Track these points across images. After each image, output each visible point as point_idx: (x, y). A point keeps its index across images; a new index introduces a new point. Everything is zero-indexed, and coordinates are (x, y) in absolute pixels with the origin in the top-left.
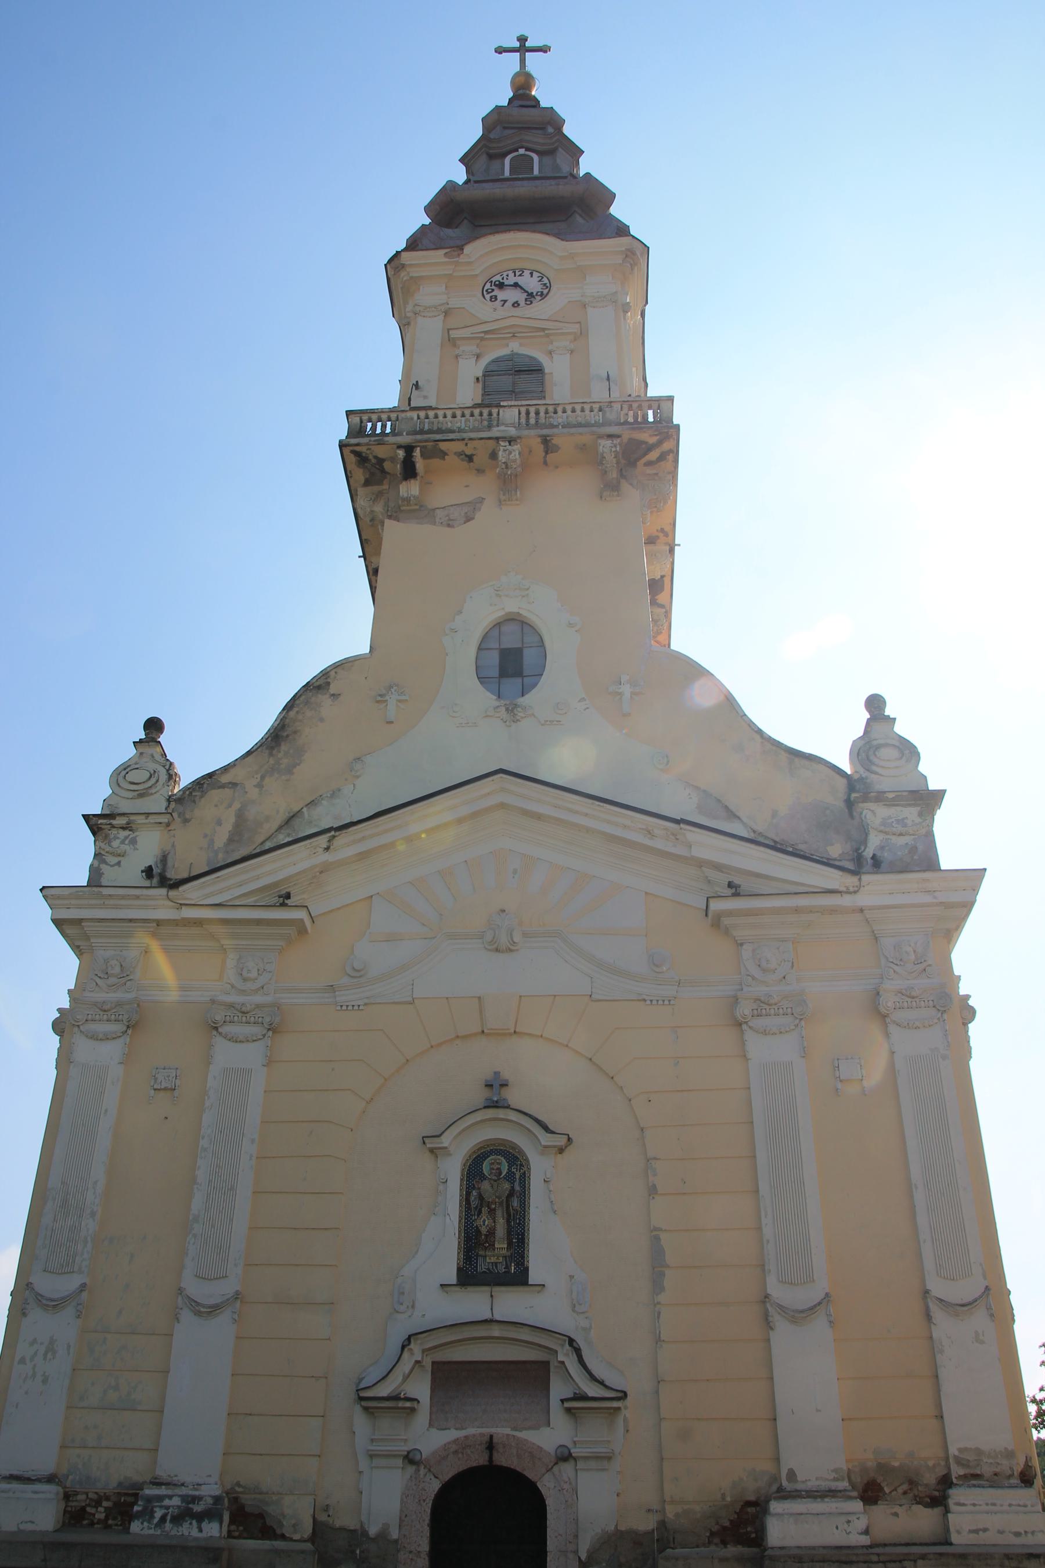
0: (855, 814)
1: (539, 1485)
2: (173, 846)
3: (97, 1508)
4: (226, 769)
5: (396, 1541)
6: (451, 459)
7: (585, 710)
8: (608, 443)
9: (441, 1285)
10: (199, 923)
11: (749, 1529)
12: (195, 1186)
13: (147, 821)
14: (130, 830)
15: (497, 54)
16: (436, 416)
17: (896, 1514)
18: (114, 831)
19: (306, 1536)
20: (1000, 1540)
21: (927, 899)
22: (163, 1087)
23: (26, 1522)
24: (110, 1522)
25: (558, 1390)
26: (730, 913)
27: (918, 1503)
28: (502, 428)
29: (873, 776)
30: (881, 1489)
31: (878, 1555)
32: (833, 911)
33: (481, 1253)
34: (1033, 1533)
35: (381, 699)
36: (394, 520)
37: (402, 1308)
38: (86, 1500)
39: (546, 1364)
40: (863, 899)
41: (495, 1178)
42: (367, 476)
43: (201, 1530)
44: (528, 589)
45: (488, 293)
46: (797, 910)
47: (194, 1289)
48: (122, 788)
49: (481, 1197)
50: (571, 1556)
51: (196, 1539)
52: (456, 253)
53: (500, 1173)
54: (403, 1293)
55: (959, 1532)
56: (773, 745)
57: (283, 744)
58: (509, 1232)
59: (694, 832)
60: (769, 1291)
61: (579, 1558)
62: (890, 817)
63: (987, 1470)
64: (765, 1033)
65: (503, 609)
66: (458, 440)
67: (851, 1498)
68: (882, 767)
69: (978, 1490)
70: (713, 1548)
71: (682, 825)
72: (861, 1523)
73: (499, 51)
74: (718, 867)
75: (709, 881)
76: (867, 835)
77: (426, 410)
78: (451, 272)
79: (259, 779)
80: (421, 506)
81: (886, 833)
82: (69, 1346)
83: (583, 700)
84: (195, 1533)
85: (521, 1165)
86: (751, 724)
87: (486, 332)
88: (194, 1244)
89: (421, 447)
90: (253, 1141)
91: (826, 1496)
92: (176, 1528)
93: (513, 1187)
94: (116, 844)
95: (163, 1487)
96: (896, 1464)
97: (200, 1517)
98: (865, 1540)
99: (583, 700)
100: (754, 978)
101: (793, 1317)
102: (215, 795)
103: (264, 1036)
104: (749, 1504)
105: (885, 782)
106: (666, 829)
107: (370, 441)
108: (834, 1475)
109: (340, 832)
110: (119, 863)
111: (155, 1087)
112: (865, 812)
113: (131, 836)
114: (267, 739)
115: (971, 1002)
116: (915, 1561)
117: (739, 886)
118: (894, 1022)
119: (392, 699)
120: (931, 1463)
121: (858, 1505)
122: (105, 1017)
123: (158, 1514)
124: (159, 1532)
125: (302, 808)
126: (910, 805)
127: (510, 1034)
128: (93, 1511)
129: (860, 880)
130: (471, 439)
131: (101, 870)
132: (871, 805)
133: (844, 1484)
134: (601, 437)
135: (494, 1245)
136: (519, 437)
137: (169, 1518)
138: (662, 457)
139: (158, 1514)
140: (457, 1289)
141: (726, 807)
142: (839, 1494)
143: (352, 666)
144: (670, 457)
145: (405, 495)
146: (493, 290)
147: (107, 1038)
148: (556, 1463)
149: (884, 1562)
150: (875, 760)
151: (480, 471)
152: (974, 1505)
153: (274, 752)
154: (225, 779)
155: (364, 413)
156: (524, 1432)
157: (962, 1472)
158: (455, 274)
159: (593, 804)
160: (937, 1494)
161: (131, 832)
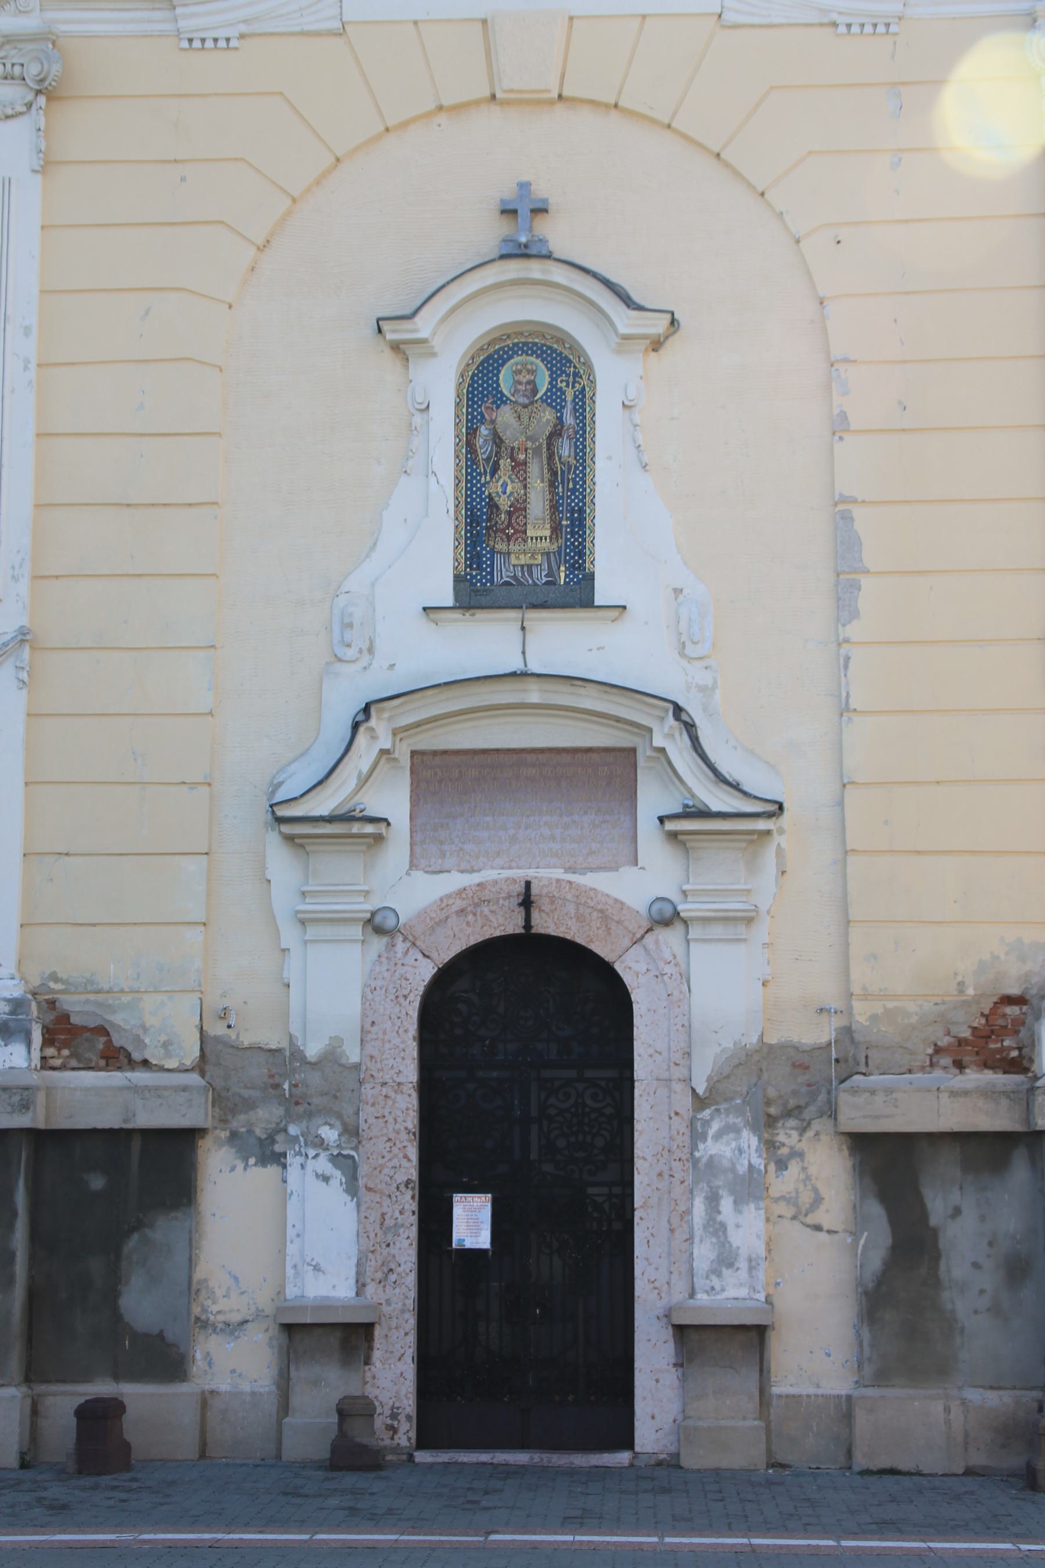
5: (357, 1067)
9: (425, 609)
11: (1006, 1043)
33: (501, 546)
37: (350, 653)
49: (497, 440)
50: (678, 1087)
53: (535, 391)
54: (350, 625)
61: (693, 1090)
70: (938, 1073)
85: (576, 375)
90: (27, 331)
93: (560, 419)
103: (29, 106)
104: (1008, 1000)
127: (550, 103)
140: (457, 615)
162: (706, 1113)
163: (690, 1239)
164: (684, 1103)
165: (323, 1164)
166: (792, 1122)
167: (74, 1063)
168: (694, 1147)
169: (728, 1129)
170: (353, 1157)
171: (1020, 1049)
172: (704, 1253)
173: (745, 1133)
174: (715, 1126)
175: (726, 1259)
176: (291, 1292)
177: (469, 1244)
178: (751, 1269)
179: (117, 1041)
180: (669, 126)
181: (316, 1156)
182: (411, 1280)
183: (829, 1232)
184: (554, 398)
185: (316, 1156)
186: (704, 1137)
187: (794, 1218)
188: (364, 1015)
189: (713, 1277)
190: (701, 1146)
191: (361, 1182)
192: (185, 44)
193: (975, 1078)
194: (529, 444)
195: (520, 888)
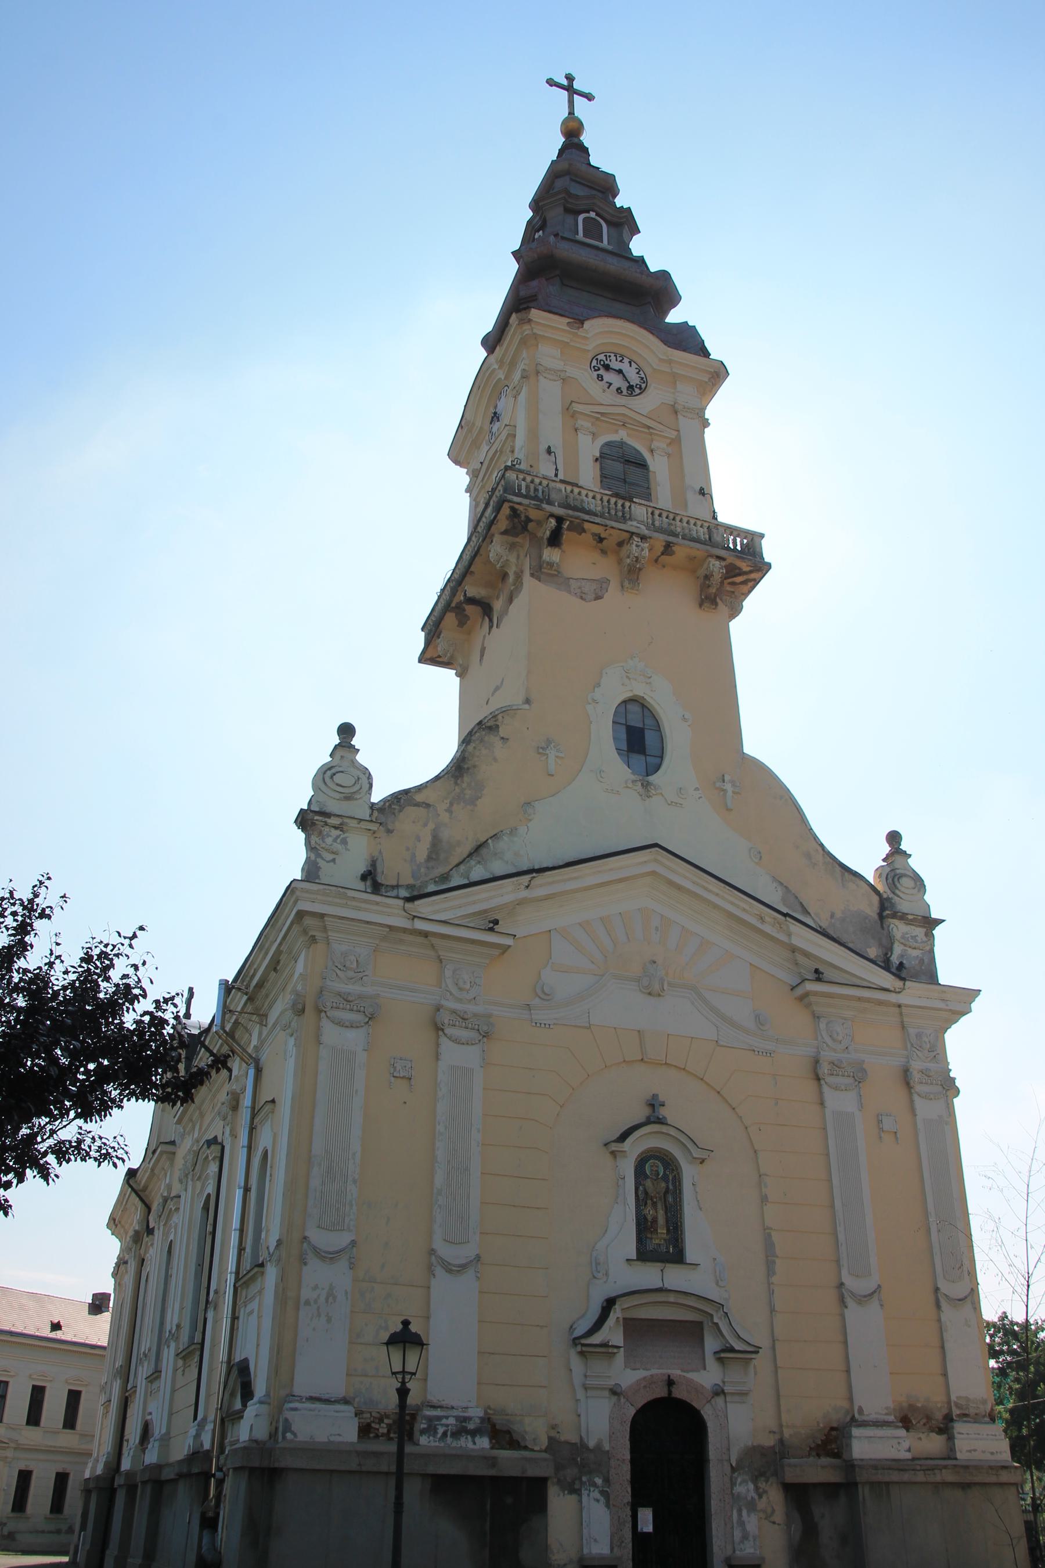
0: (884, 925)
1: (702, 1412)
2: (380, 852)
3: (380, 1424)
4: (420, 788)
5: (608, 1451)
6: (587, 537)
7: (699, 798)
9: (627, 1260)
10: (426, 934)
11: (833, 1446)
12: (436, 1165)
13: (359, 826)
14: (341, 831)
15: (547, 85)
16: (579, 493)
17: (920, 1439)
18: (326, 829)
19: (544, 1447)
20: (983, 1457)
21: (941, 1005)
22: (401, 1076)
23: (335, 1435)
24: (392, 1435)
25: (711, 1344)
26: (816, 994)
27: (932, 1431)
28: (634, 523)
29: (896, 897)
30: (910, 1422)
31: (921, 1465)
32: (880, 1003)
33: (649, 1235)
34: (1001, 1453)
35: (541, 750)
36: (536, 579)
37: (600, 1275)
38: (370, 1418)
39: (699, 1325)
40: (903, 999)
41: (654, 1178)
42: (509, 528)
43: (475, 1443)
44: (650, 677)
45: (595, 370)
46: (860, 999)
47: (444, 1251)
48: (329, 787)
49: (646, 1193)
50: (725, 1463)
51: (473, 1450)
52: (577, 325)
53: (658, 1175)
54: (599, 1264)
55: (961, 1452)
56: (831, 858)
57: (465, 775)
58: (667, 1221)
59: (795, 925)
60: (844, 1280)
61: (731, 1465)
62: (907, 934)
63: (972, 1411)
64: (836, 1088)
65: (632, 691)
66: (602, 525)
67: (897, 1427)
68: (903, 893)
69: (970, 1425)
70: (811, 1459)
71: (788, 918)
72: (906, 1445)
73: (550, 83)
74: (806, 954)
75: (797, 964)
76: (892, 944)
77: (573, 486)
78: (569, 341)
79: (448, 805)
80: (559, 572)
81: (905, 945)
82: (346, 1293)
83: (697, 789)
84: (470, 1445)
85: (673, 1170)
86: (815, 838)
87: (602, 414)
88: (440, 1213)
89: (571, 522)
90: (479, 1131)
91: (885, 1425)
92: (455, 1442)
93: (668, 1186)
94: (329, 840)
95: (439, 1409)
96: (919, 1405)
97: (473, 1433)
98: (908, 1456)
99: (697, 789)
101: (859, 1300)
102: (410, 810)
103: (480, 1041)
104: (832, 1429)
106: (774, 918)
107: (530, 503)
108: (885, 1411)
109: (537, 875)
110: (334, 860)
111: (395, 1075)
112: (892, 926)
113: (342, 836)
114: (451, 768)
116: (941, 1470)
117: (823, 974)
118: (916, 1093)
119: (552, 753)
120: (939, 1405)
121: (902, 1432)
123: (441, 1430)
124: (442, 1444)
125: (488, 840)
126: (920, 926)
127: (662, 1064)
128: (377, 1426)
129: (904, 984)
130: (612, 528)
131: (318, 864)
132: (896, 922)
133: (891, 1418)
134: (711, 556)
135: (657, 1230)
136: (650, 538)
137: (449, 1433)
139: (441, 1430)
140: (639, 1263)
141: (801, 903)
142: (892, 1425)
143: (515, 714)
144: (750, 584)
145: (548, 559)
146: (599, 369)
147: (352, 1026)
148: (713, 1397)
149: (923, 1470)
150: (898, 885)
151: (604, 552)
152: (968, 1434)
153: (459, 781)
154: (419, 798)
155: (521, 472)
156: (691, 1373)
157: (958, 1413)
158: (572, 344)
159: (724, 887)
160: (942, 1425)
161: (341, 833)
162: (736, 1474)
163: (732, 1528)
164: (728, 1470)
165: (596, 1494)
166: (763, 1479)
167: (497, 1446)
168: (732, 1489)
169: (744, 1481)
170: (607, 1491)
171: (837, 1448)
172: (737, 1534)
173: (750, 1483)
174: (739, 1480)
175: (745, 1537)
176: (585, 1551)
177: (645, 1530)
178: (754, 1540)
179: (515, 1437)
180: (702, 1079)
181: (593, 1491)
182: (630, 1545)
183: (778, 1524)
184: (665, 1178)
185: (593, 1491)
186: (735, 1484)
187: (766, 1519)
188: (610, 1429)
189: (741, 1544)
190: (735, 1488)
191: (611, 1502)
192: (534, 1024)
193: (825, 1460)
194: (657, 1195)
195: (666, 1378)
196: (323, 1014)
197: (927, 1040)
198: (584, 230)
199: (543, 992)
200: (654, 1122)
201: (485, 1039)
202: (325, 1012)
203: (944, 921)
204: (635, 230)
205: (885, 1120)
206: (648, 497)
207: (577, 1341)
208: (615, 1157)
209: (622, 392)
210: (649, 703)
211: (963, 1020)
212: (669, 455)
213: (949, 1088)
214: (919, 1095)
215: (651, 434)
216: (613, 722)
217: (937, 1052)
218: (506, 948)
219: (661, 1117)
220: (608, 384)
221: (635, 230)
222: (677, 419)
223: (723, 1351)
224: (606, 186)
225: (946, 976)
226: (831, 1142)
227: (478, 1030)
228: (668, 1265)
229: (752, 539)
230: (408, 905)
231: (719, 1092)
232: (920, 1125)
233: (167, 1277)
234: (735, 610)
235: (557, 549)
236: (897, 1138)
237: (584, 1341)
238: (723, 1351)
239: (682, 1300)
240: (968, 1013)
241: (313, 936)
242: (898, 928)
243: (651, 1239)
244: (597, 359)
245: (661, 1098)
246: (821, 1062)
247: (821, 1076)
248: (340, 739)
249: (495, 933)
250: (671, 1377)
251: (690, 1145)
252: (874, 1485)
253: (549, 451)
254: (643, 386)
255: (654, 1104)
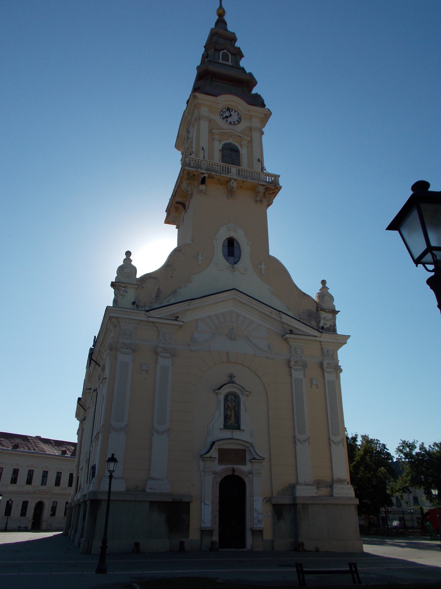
1: (244, 480)
8: (262, 187)
9: (220, 429)
10: (153, 322)
18: (120, 288)
21: (336, 341)
29: (322, 303)
33: (228, 421)
40: (321, 339)
44: (236, 230)
45: (222, 115)
49: (228, 406)
53: (232, 400)
58: (235, 416)
59: (283, 315)
68: (324, 301)
71: (280, 313)
74: (288, 325)
85: (238, 398)
87: (223, 133)
93: (236, 404)
94: (121, 292)
100: (294, 356)
105: (324, 306)
112: (321, 313)
115: (341, 368)
117: (293, 331)
122: (126, 348)
127: (241, 364)
132: (322, 312)
138: (273, 193)
144: (275, 193)
161: (125, 289)
176: (202, 526)
184: (235, 402)
192: (191, 351)
194: (232, 407)
195: (232, 468)
196: (118, 350)
197: (330, 353)
198: (222, 55)
199: (194, 340)
200: (231, 383)
201: (173, 357)
202: (119, 349)
203: (340, 311)
204: (242, 56)
205: (314, 381)
206: (239, 164)
207: (202, 456)
208: (217, 395)
209: (231, 123)
210: (236, 239)
211: (344, 346)
212: (248, 147)
213: (338, 369)
214: (326, 372)
215: (241, 139)
216: (223, 246)
217: (334, 357)
218: (181, 326)
219: (233, 381)
220: (226, 121)
221: (242, 56)
222: (251, 133)
223: (252, 459)
224: (232, 39)
225: (340, 330)
226: (294, 389)
227: (171, 354)
228: (234, 430)
229: (275, 177)
230: (147, 313)
231: (254, 372)
232: (326, 383)
233: (103, 402)
234: (269, 204)
235: (204, 185)
236: (318, 387)
237: (203, 456)
238: (252, 459)
239: (238, 442)
240: (346, 344)
241: (115, 324)
242: (323, 314)
243: (229, 422)
244: (223, 111)
245: (234, 375)
246: (291, 361)
247: (291, 366)
248: (126, 256)
249: (178, 321)
250: (234, 468)
251: (243, 390)
252: (303, 505)
253: (203, 149)
254: (239, 120)
255: (231, 376)
